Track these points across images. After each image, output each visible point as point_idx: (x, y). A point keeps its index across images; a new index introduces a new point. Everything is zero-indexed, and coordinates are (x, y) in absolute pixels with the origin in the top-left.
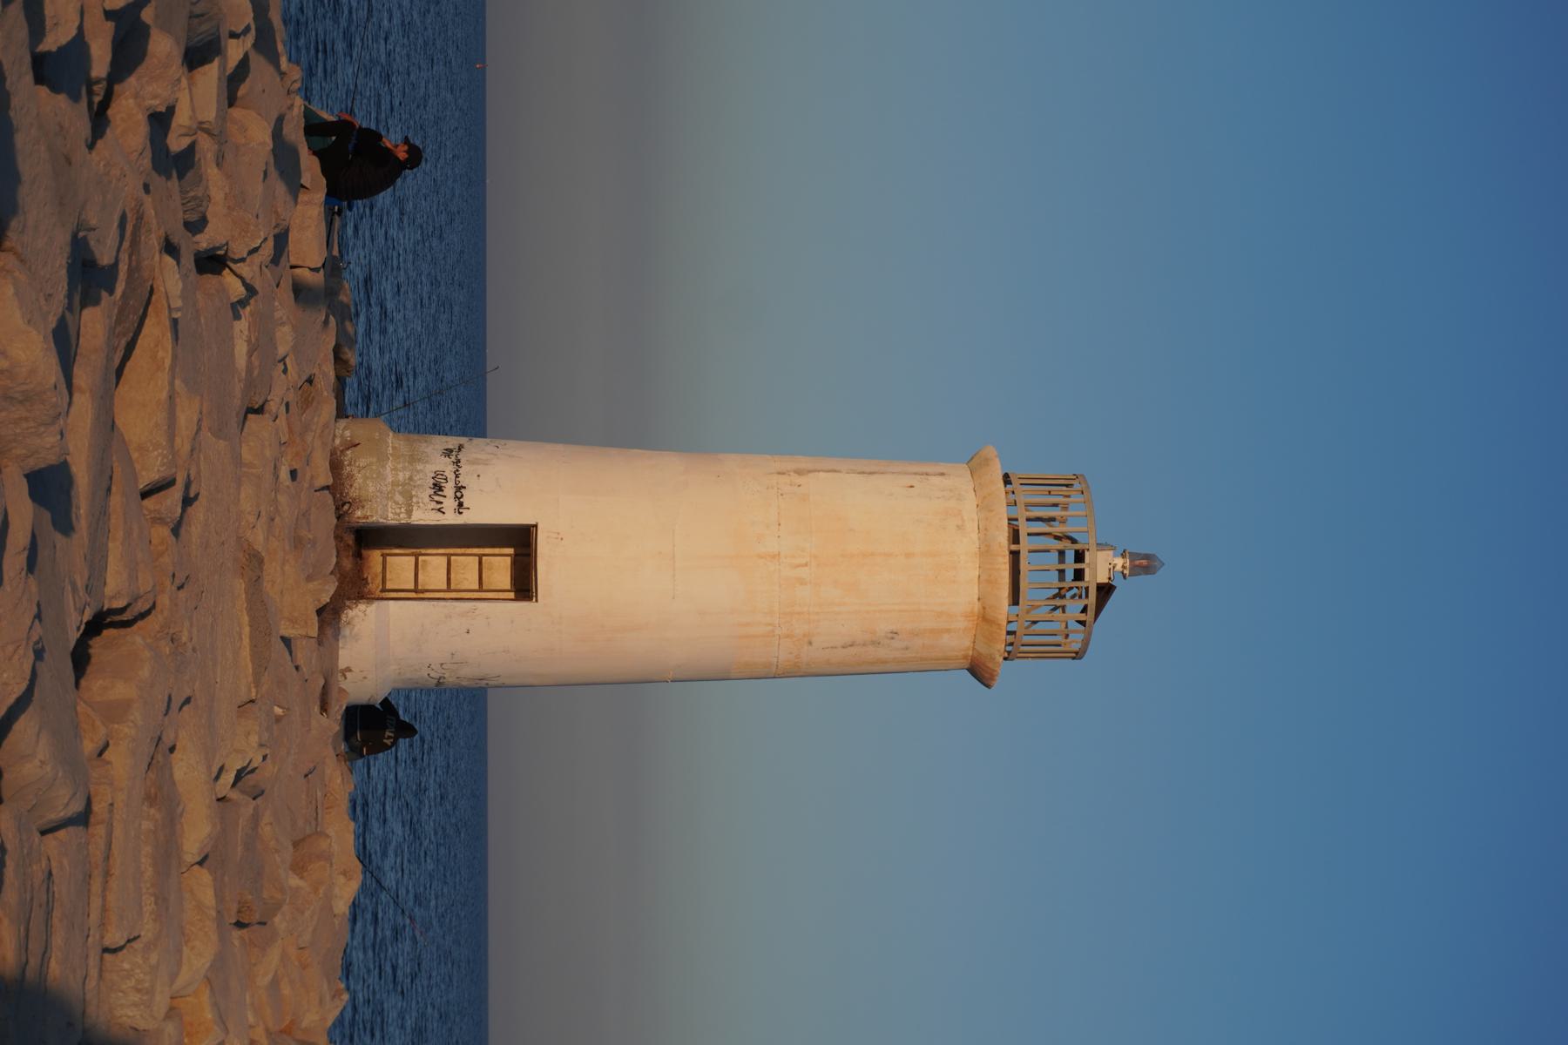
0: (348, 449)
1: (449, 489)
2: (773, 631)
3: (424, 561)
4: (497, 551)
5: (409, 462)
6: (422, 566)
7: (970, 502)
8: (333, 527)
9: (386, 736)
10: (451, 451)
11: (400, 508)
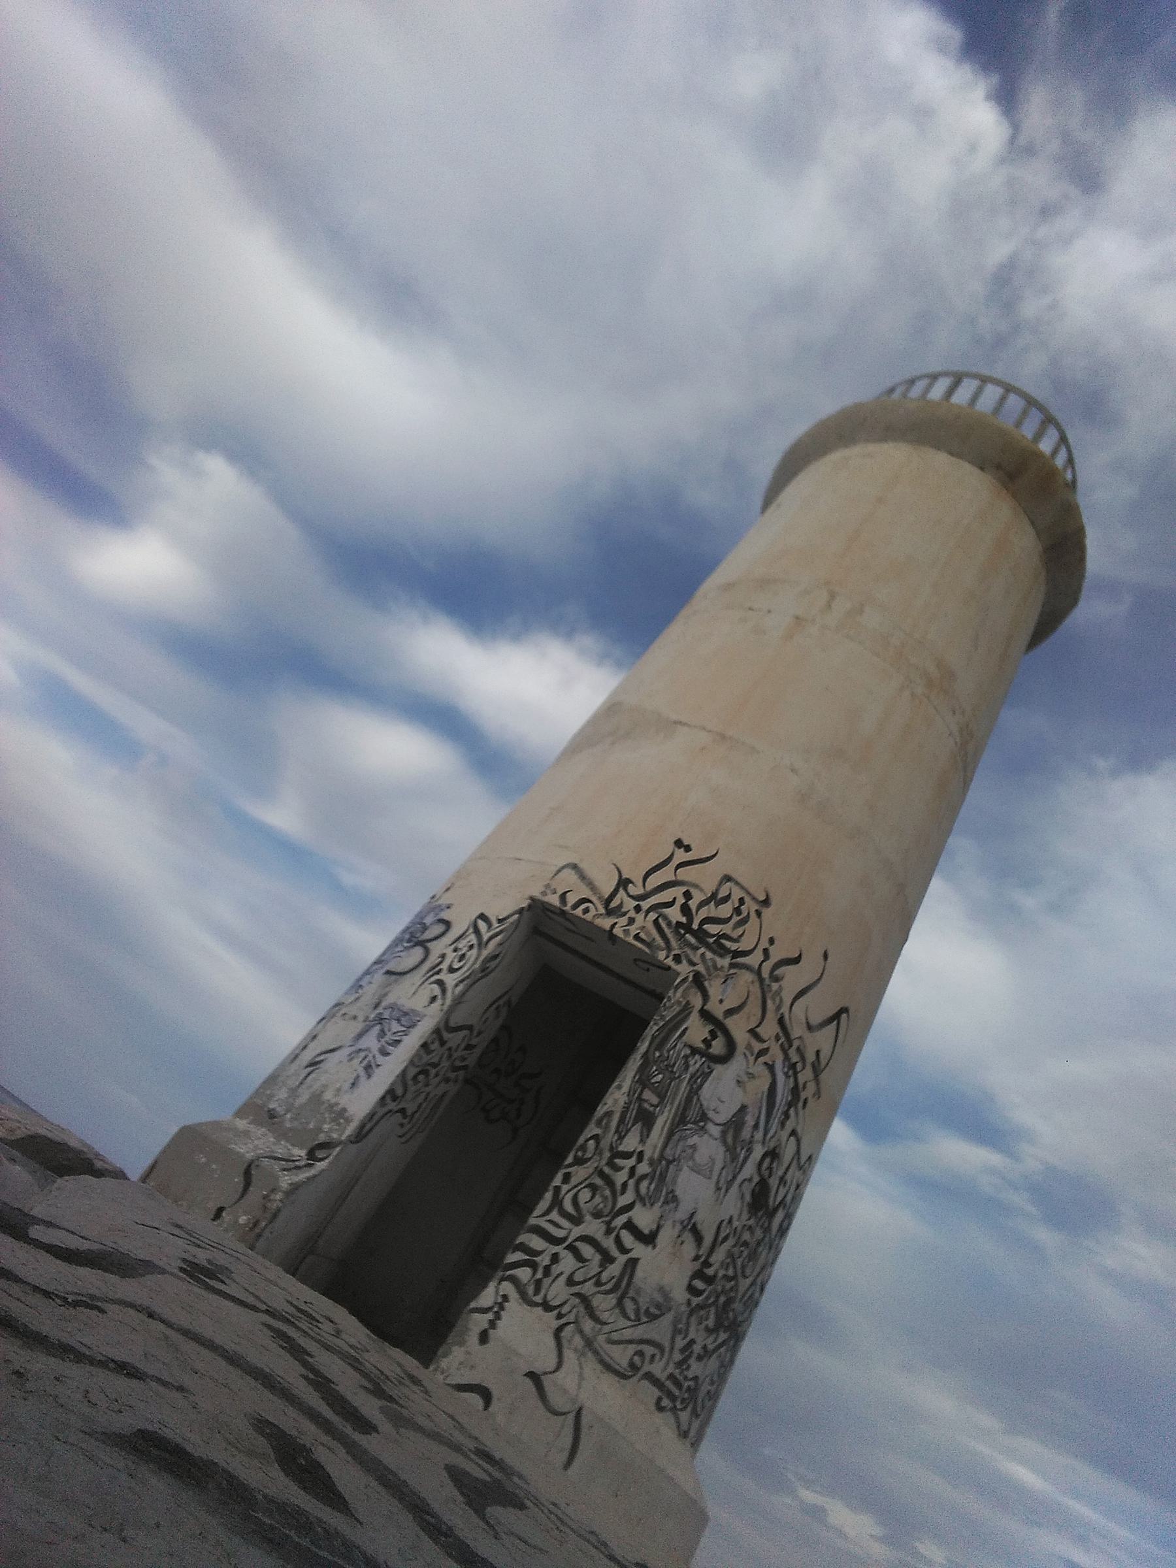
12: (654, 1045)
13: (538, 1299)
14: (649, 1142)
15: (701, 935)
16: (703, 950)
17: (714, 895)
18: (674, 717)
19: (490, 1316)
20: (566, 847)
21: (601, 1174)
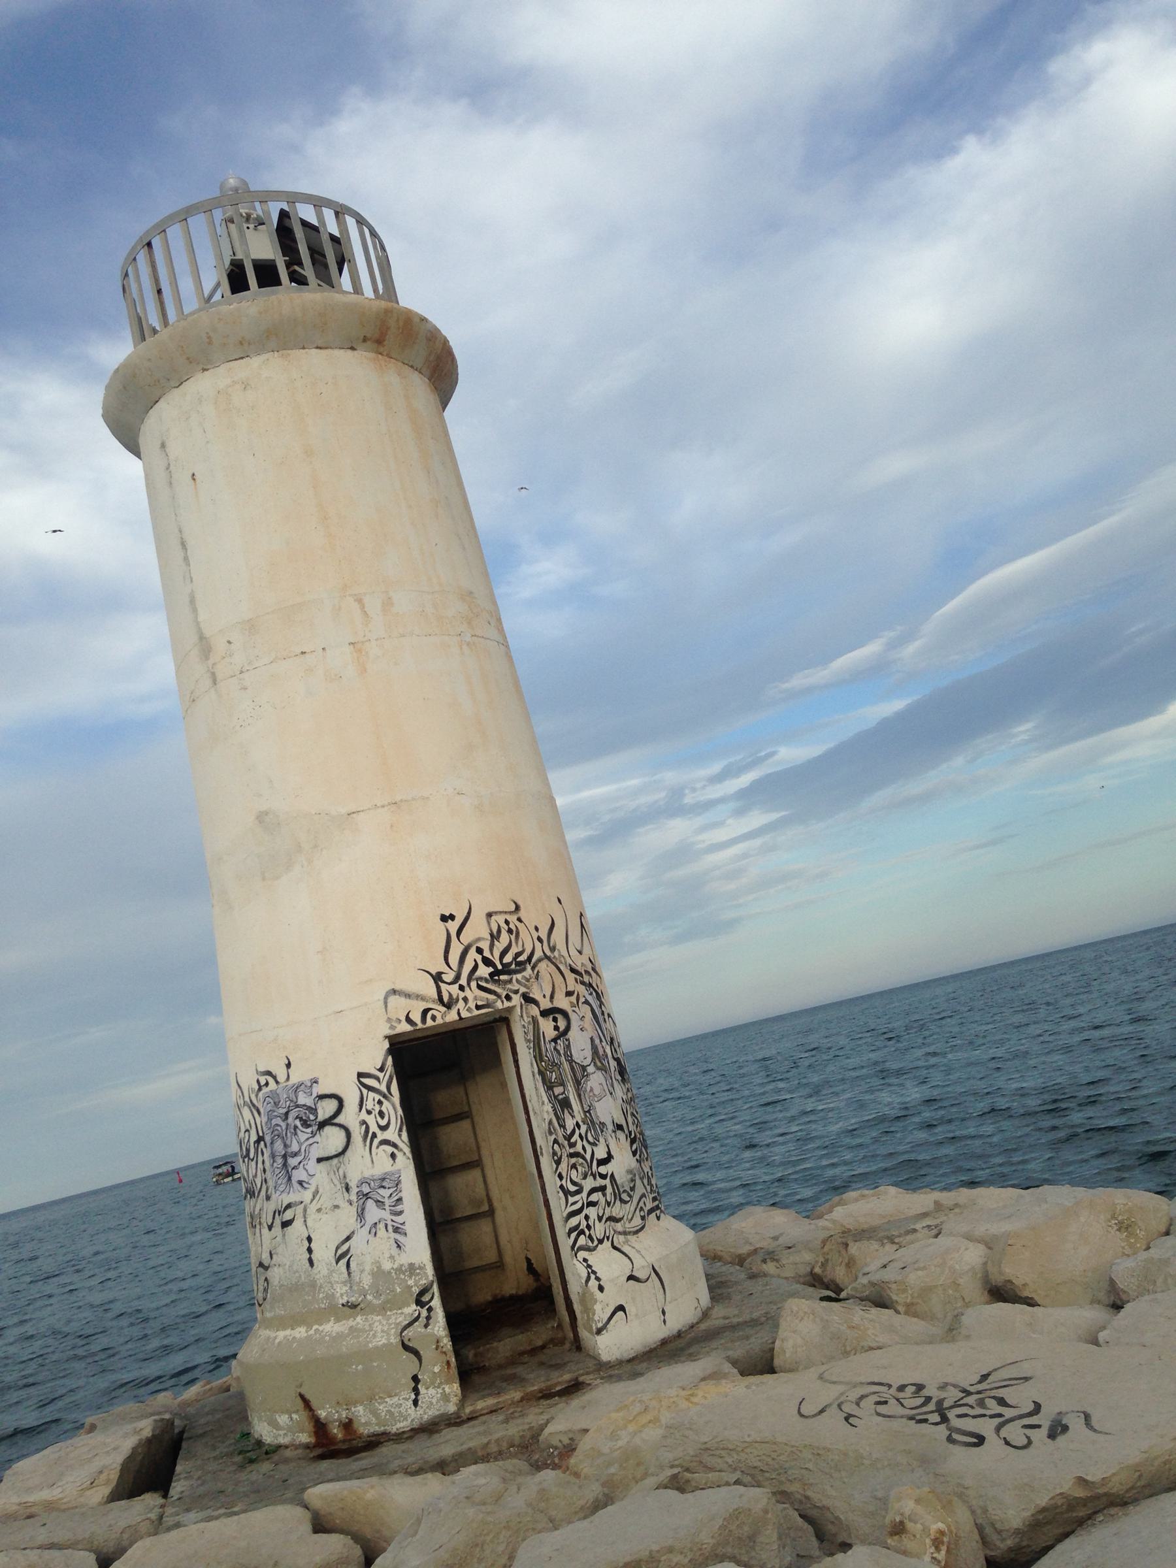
12: (539, 1062)
13: (596, 1242)
14: (576, 1113)
15: (506, 969)
16: (514, 977)
17: (492, 935)
18: (344, 811)
19: (593, 1276)
20: (371, 980)
21: (572, 1155)
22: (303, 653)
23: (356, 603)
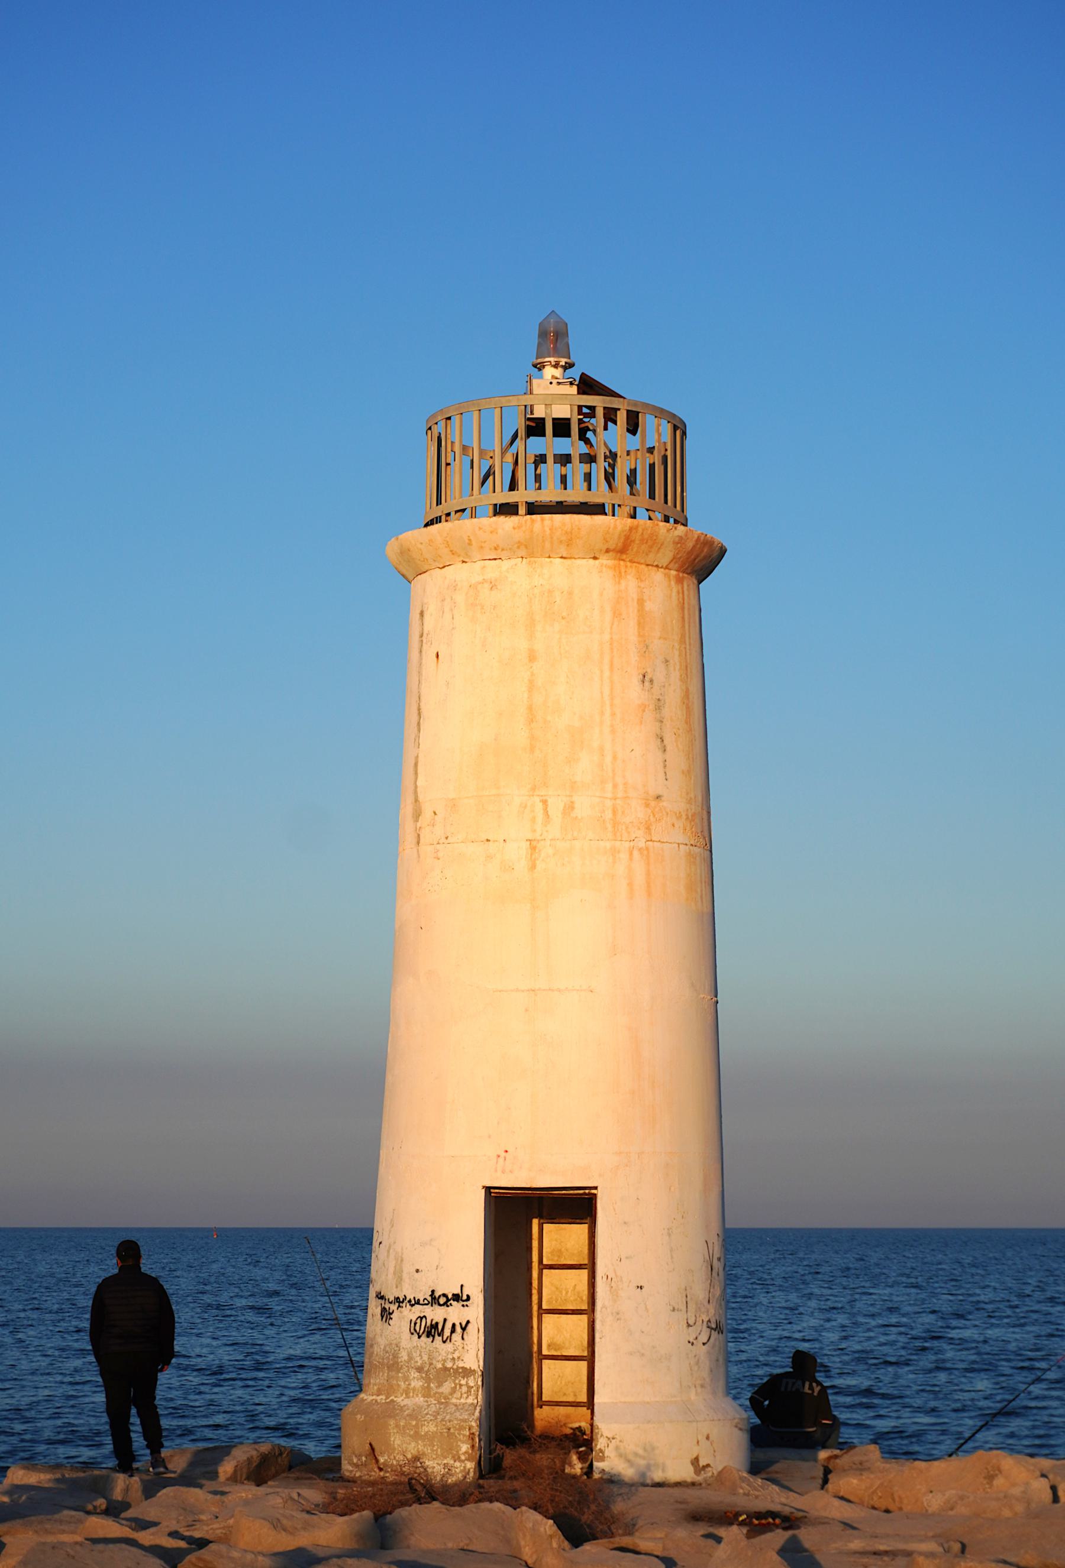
0: (377, 1461)
1: (435, 1314)
2: (640, 850)
3: (549, 1346)
4: (535, 1244)
5: (398, 1371)
6: (556, 1350)
7: (458, 573)
8: (444, 1508)
9: (810, 1392)
10: (384, 1310)
11: (461, 1385)
22: (488, 840)
23: (541, 804)
